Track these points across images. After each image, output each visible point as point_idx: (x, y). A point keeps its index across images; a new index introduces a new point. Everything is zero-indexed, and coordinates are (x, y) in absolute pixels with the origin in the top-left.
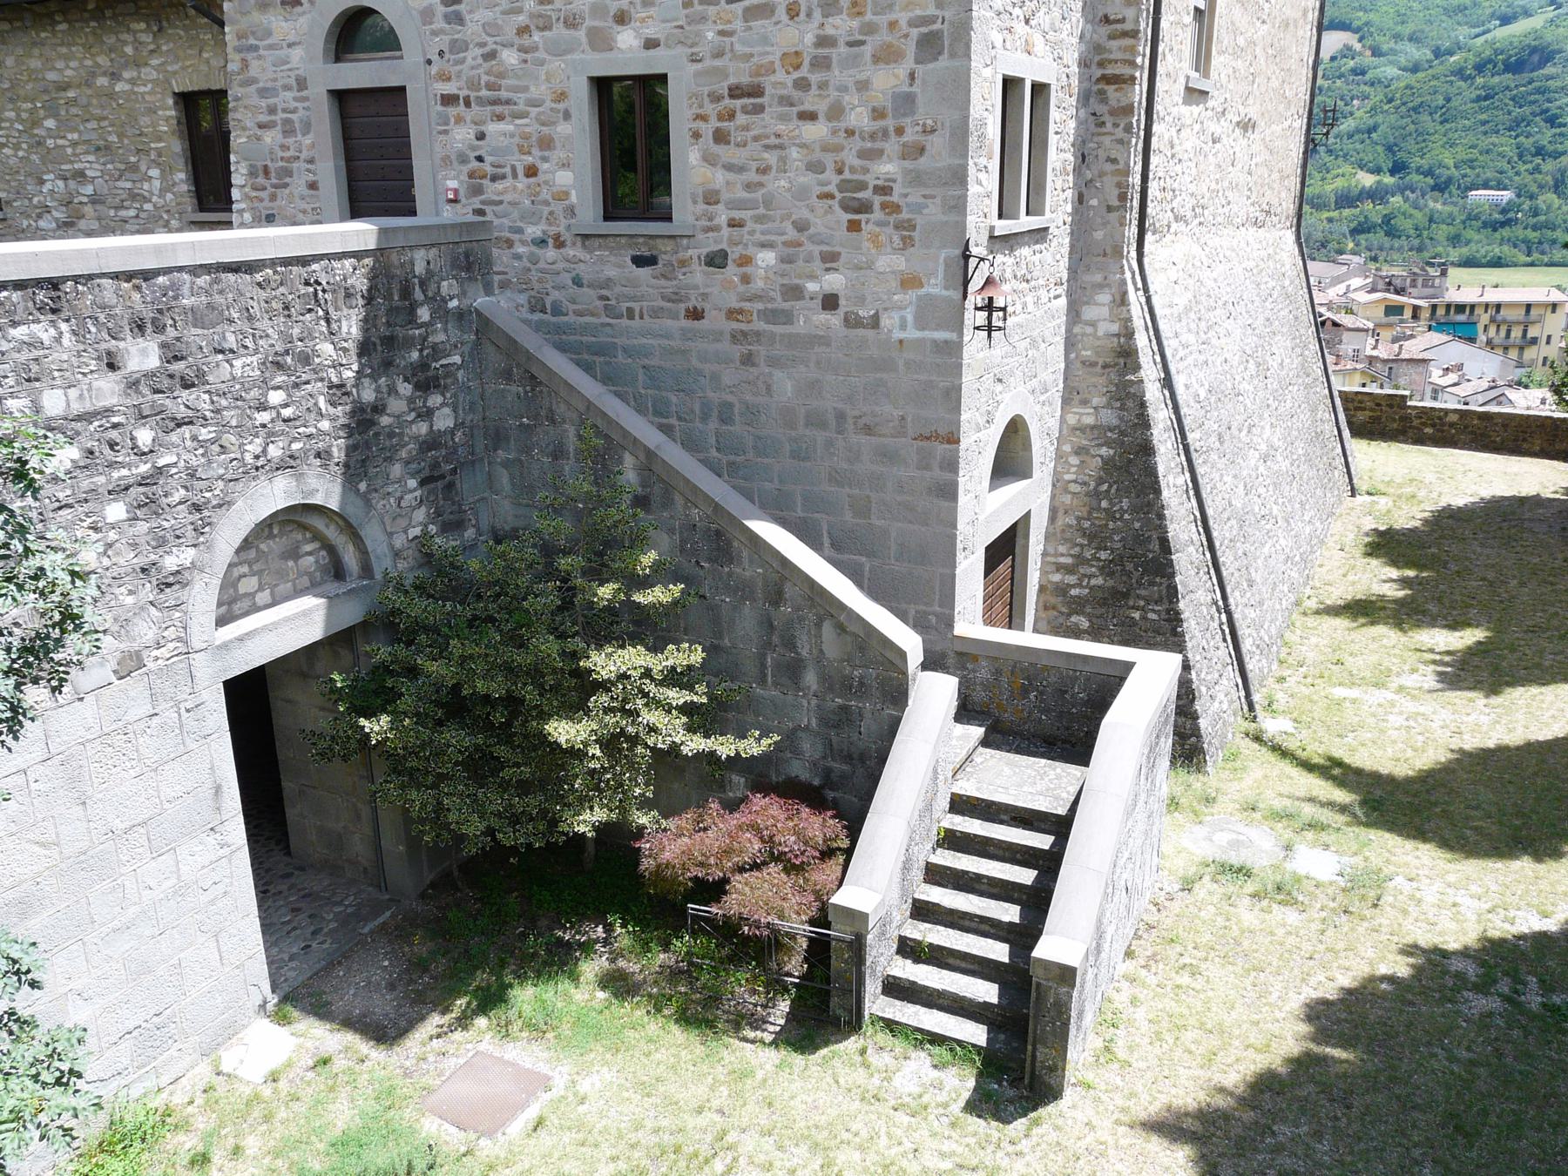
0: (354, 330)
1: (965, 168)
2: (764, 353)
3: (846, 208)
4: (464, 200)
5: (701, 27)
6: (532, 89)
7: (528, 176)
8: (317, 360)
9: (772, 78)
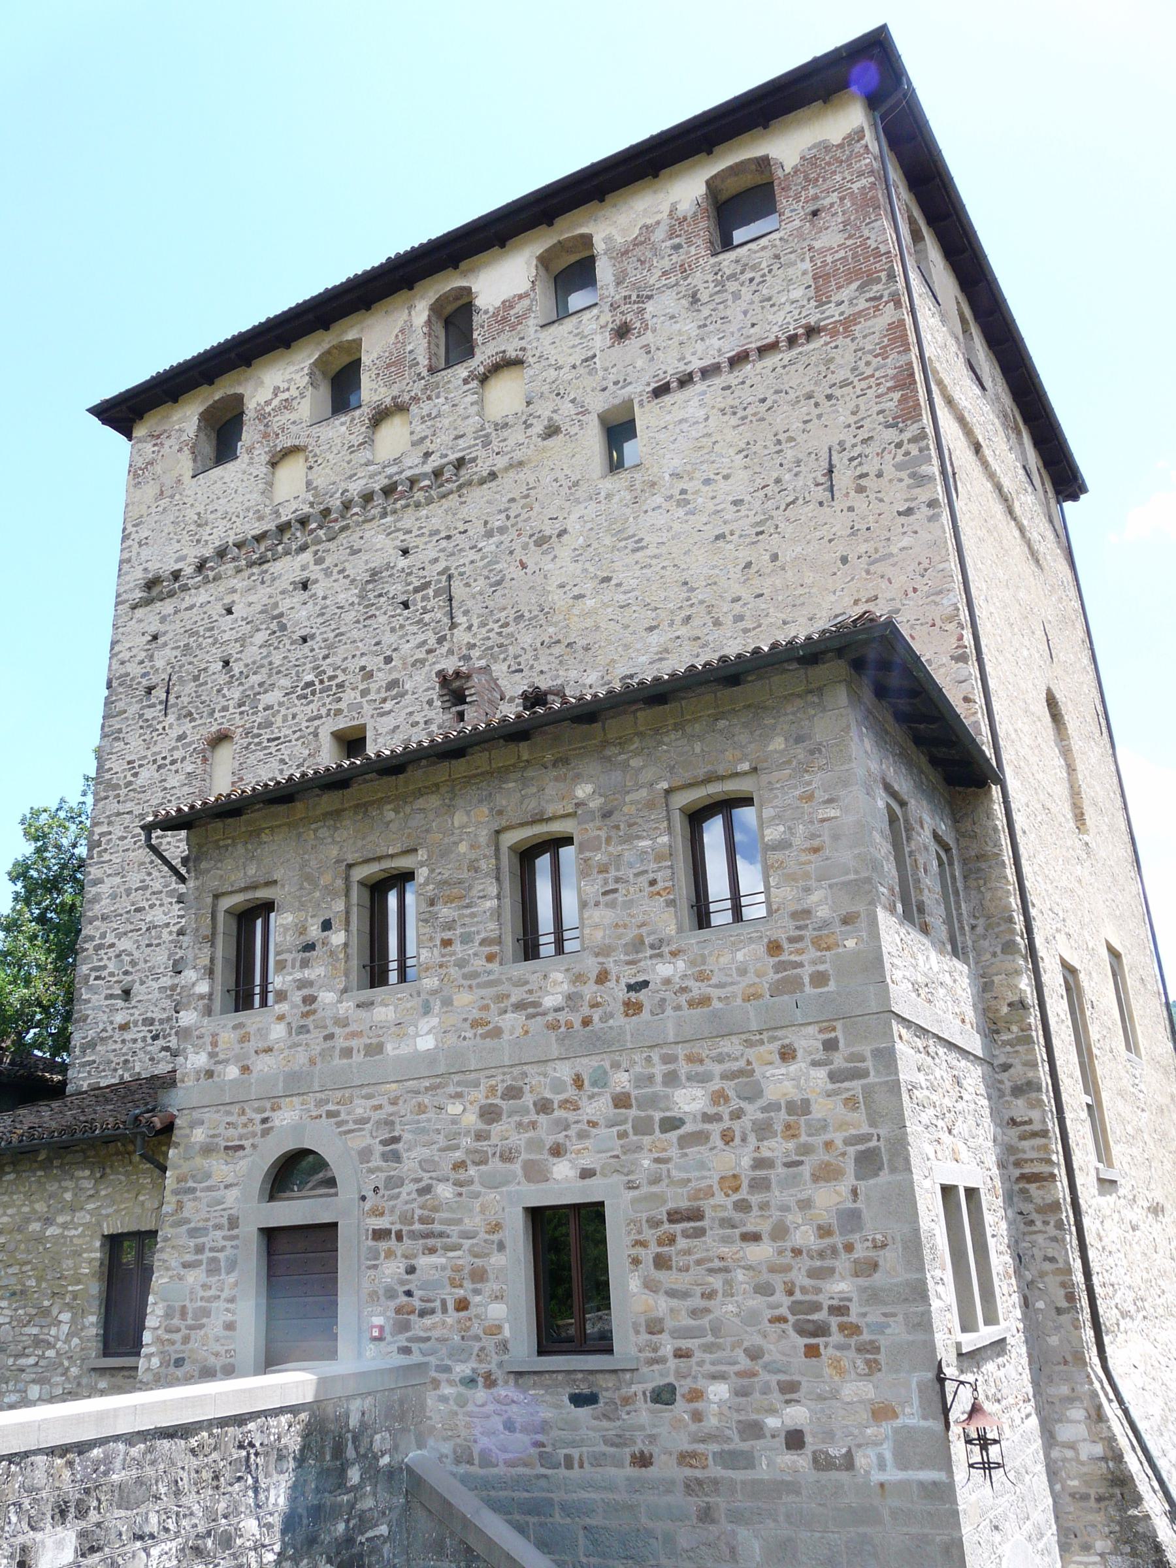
0: (282, 1501)
1: (924, 1282)
2: (723, 1506)
3: (801, 1332)
4: (389, 1338)
5: (636, 1155)
6: (466, 1221)
7: (458, 1310)
8: (239, 1542)
9: (712, 1201)
